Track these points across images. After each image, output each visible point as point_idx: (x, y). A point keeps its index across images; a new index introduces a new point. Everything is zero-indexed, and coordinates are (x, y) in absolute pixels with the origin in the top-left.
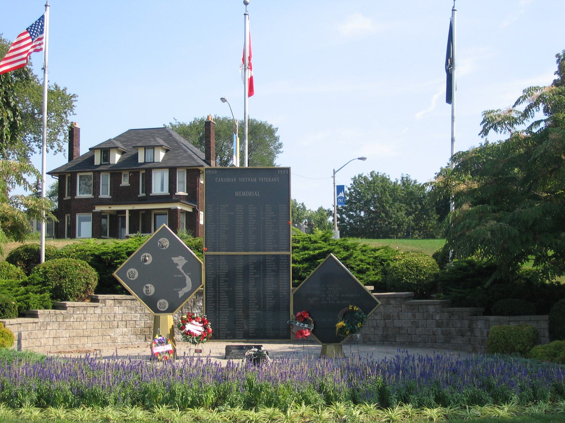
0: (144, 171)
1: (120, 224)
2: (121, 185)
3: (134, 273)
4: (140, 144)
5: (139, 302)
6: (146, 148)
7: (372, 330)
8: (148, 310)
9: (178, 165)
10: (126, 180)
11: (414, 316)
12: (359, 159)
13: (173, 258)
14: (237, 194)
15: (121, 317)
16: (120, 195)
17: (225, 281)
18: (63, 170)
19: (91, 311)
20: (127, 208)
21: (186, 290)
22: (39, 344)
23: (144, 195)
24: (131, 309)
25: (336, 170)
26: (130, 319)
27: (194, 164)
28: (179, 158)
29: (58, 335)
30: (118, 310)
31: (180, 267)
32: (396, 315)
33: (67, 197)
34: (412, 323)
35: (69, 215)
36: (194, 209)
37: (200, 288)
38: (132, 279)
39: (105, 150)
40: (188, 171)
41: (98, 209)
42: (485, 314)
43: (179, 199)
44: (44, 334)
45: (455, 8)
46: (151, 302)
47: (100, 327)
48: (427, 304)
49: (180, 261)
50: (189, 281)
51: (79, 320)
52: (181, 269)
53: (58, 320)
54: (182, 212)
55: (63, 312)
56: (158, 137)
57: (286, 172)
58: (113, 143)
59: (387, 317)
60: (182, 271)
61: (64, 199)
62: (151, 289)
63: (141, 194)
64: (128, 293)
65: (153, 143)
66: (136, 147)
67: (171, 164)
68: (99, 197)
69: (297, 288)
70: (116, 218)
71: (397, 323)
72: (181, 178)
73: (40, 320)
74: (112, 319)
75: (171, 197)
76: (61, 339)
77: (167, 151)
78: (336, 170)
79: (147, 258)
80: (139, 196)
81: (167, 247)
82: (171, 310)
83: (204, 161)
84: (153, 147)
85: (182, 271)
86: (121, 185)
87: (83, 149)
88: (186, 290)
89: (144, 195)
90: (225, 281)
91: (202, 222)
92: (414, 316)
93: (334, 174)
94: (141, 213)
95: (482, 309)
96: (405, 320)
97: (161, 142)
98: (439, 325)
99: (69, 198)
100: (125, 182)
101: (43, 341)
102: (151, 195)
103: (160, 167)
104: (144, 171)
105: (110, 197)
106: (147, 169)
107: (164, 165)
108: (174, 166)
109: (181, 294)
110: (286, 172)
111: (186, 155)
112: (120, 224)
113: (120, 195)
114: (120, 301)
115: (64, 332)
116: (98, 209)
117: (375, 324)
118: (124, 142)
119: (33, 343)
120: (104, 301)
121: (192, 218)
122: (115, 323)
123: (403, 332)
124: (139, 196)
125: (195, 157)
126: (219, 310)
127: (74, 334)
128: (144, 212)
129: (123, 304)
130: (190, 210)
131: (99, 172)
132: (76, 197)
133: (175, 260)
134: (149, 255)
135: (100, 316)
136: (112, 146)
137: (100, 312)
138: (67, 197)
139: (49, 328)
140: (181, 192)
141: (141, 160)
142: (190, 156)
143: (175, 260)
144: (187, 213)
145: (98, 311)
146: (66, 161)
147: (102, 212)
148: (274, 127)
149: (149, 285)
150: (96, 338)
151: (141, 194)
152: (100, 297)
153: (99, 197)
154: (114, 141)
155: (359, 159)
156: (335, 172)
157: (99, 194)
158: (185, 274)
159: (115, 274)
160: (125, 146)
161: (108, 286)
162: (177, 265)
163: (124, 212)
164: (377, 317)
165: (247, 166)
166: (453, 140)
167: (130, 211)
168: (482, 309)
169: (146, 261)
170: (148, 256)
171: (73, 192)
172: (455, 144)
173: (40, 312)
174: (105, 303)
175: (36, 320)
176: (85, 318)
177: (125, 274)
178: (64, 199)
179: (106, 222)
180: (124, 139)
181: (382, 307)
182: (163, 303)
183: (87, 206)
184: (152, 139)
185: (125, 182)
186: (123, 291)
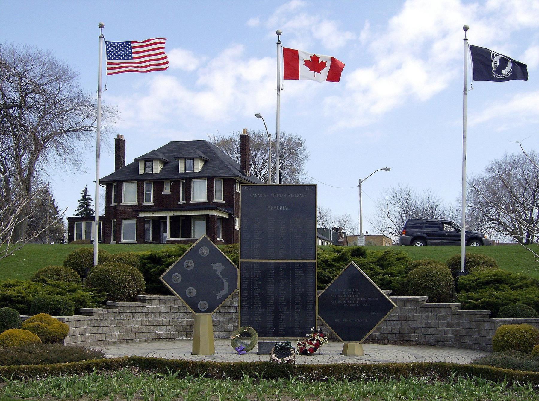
0: (184, 181)
1: (162, 229)
2: (163, 193)
3: (178, 277)
4: (180, 156)
5: (181, 302)
6: (186, 159)
7: (390, 329)
8: (190, 310)
9: (215, 175)
10: (167, 188)
11: (428, 317)
12: (383, 169)
13: (212, 264)
14: (269, 208)
15: (165, 315)
16: (162, 202)
17: (258, 285)
18: (110, 179)
19: (139, 310)
20: (169, 214)
21: (224, 292)
22: (93, 339)
23: (184, 202)
24: (174, 308)
25: (362, 180)
26: (173, 318)
27: (230, 174)
28: (217, 169)
29: (110, 331)
30: (163, 309)
31: (218, 273)
32: (411, 316)
33: (113, 204)
34: (426, 324)
35: (115, 220)
36: (230, 216)
37: (236, 290)
38: (176, 283)
39: (148, 159)
40: (225, 180)
41: (142, 215)
42: (491, 316)
43: (215, 207)
44: (98, 330)
45: (467, 38)
46: (193, 304)
47: (146, 324)
48: (440, 307)
49: (218, 267)
50: (226, 284)
51: (128, 317)
52: (219, 274)
53: (110, 318)
54: (219, 218)
55: (114, 310)
56: (197, 149)
57: (311, 190)
58: (156, 154)
59: (403, 318)
60: (221, 276)
61: (111, 205)
62: (192, 292)
63: (182, 202)
64: (172, 294)
65: (192, 155)
66: (178, 159)
67: (210, 173)
68: (143, 204)
69: (322, 291)
70: (159, 223)
71: (412, 324)
72: (219, 188)
73: (95, 317)
74: (158, 317)
75: (210, 205)
76: (112, 334)
77: (206, 162)
78: (362, 180)
79: (190, 264)
80: (179, 203)
81: (207, 254)
82: (210, 310)
83: (239, 171)
84: (192, 159)
85: (221, 276)
86: (163, 193)
87: (129, 160)
88: (224, 292)
89: (184, 202)
90: (258, 285)
91: (237, 228)
92: (428, 317)
93: (360, 184)
94: (181, 219)
95: (489, 312)
96: (419, 321)
97: (201, 154)
98: (450, 325)
99: (116, 204)
100: (167, 190)
101: (97, 336)
102: (190, 202)
103: (198, 176)
104: (184, 181)
105: (153, 204)
106: (186, 179)
107: (202, 175)
108: (212, 175)
109: (219, 296)
110: (311, 190)
111: (223, 166)
112: (162, 229)
113: (162, 202)
114: (164, 302)
115: (115, 328)
116: (142, 215)
117: (392, 324)
118: (166, 153)
119: (88, 338)
120: (151, 301)
121: (228, 223)
122: (160, 321)
123: (418, 332)
124: (179, 203)
125: (231, 167)
126: (253, 309)
127: (124, 330)
128: (184, 218)
129: (167, 304)
130: (226, 216)
131: (143, 181)
132: (121, 204)
133: (214, 266)
134: (192, 261)
135: (147, 314)
136: (155, 157)
137: (147, 311)
138: (113, 204)
139: (102, 324)
140: (219, 198)
141: (182, 170)
142: (227, 167)
143: (214, 266)
144: (224, 219)
145: (145, 310)
146: (112, 170)
147: (146, 217)
148: (302, 139)
149: (191, 288)
150: (143, 334)
151: (182, 202)
152: (148, 297)
153: (143, 204)
154: (157, 153)
155: (383, 169)
156: (361, 182)
157: (143, 202)
158: (222, 279)
159: (161, 277)
160: (167, 157)
161: (156, 287)
162: (216, 270)
163: (166, 218)
164: (394, 319)
165: (278, 183)
166: (465, 159)
167: (172, 217)
168: (489, 312)
169: (189, 267)
170: (191, 263)
171: (119, 198)
172: (226, 383)
173: (95, 310)
174: (151, 303)
175: (91, 317)
176: (134, 316)
177: (169, 277)
178: (111, 205)
179: (149, 227)
180: (166, 151)
181: (398, 310)
182: (203, 304)
183: (131, 211)
184: (192, 151)
185: (167, 190)
186: (167, 292)
